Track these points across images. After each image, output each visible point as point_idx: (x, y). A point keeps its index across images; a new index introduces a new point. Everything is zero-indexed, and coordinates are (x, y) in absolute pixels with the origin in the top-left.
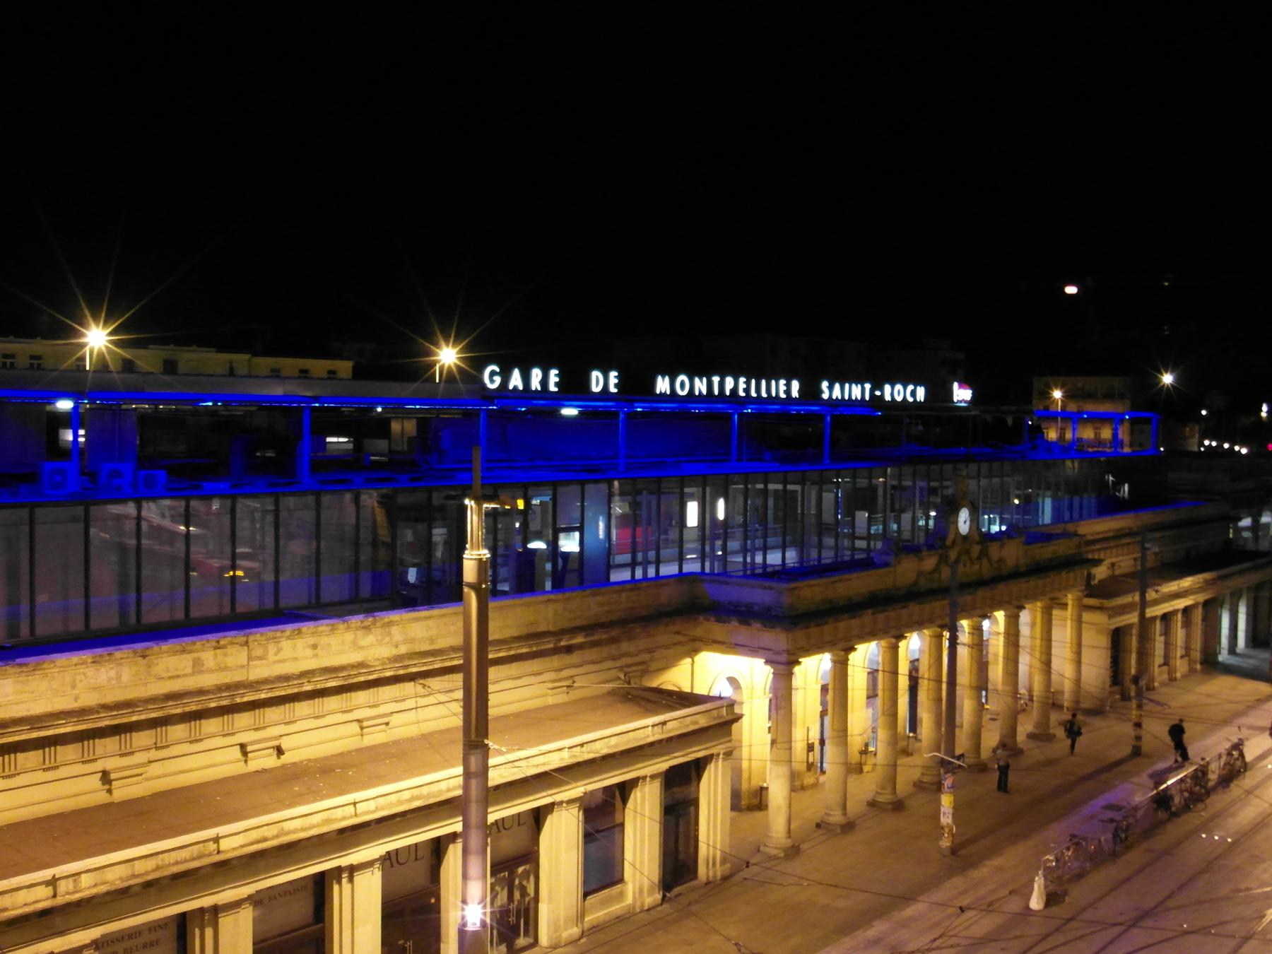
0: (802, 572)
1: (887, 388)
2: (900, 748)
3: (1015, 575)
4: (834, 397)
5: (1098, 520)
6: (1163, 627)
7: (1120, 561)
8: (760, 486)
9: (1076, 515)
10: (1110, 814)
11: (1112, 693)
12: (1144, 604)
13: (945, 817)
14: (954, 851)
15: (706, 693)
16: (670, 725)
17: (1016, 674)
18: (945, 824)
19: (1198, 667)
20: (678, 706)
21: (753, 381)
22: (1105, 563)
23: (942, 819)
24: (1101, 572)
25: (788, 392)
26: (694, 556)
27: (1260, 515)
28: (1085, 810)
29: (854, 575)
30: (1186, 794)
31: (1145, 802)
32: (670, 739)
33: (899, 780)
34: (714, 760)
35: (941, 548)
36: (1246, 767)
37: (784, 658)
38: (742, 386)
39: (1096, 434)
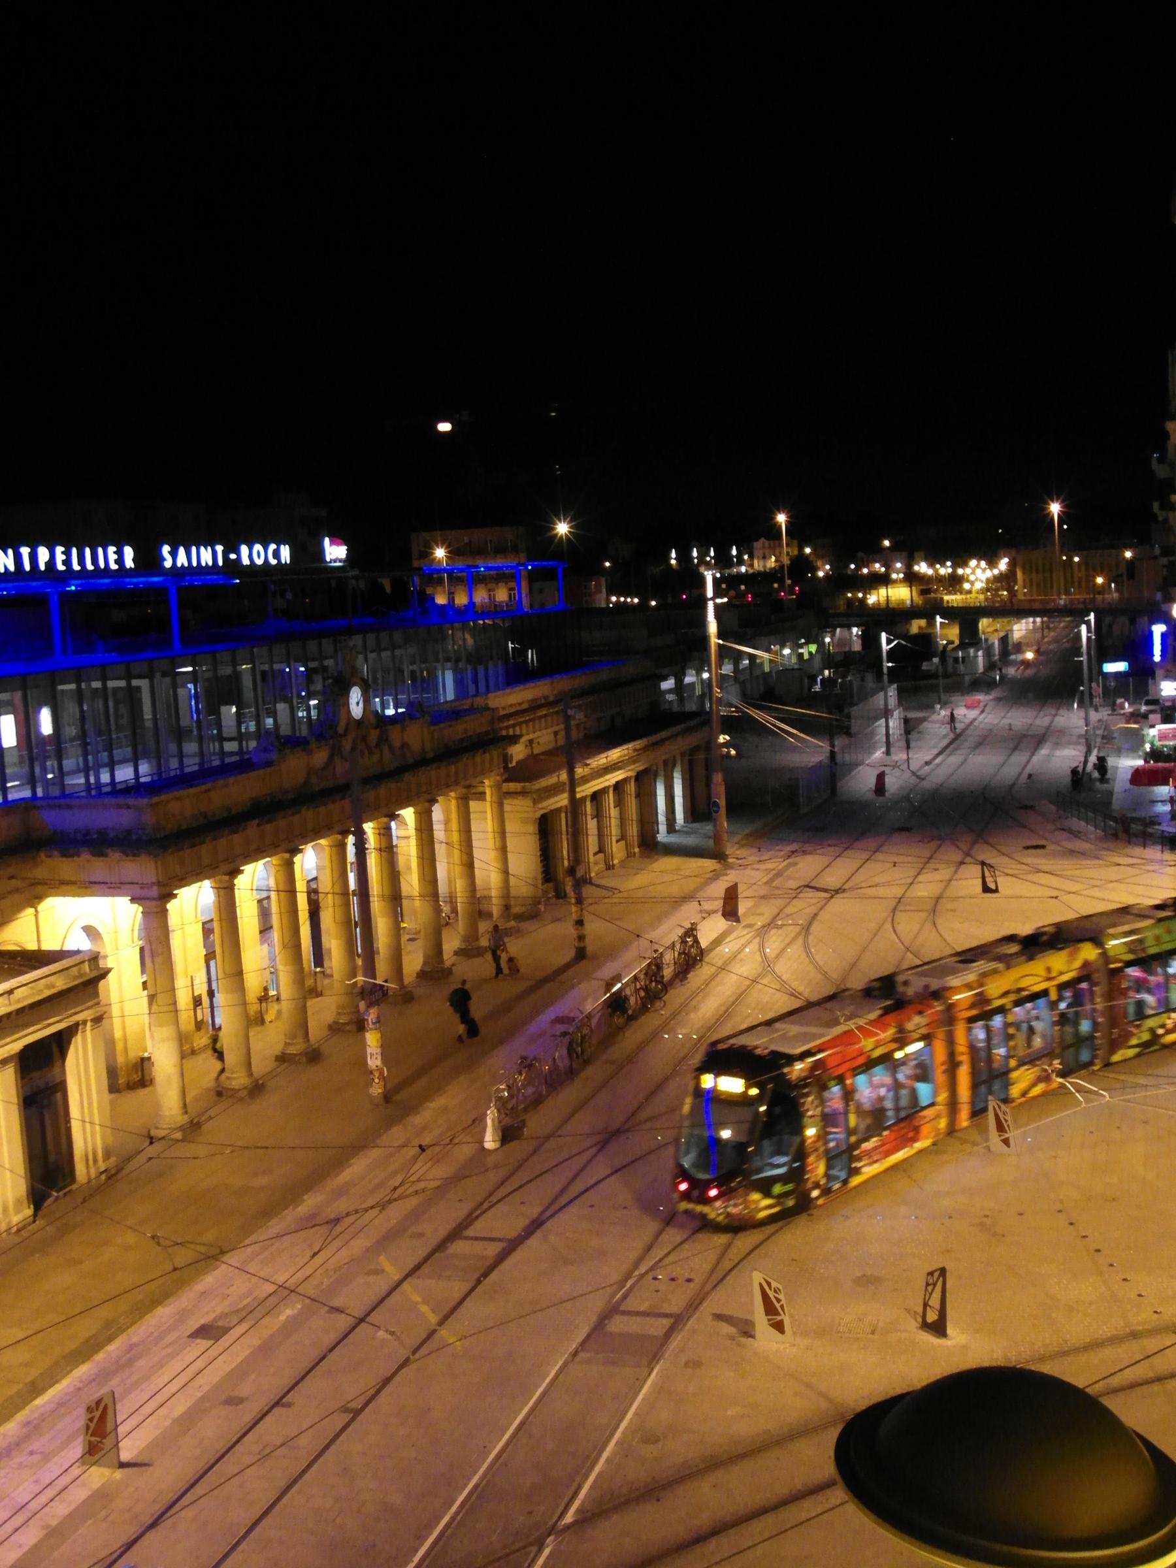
0: (160, 785)
1: (244, 549)
2: (308, 991)
3: (423, 762)
4: (179, 565)
5: (508, 691)
6: (595, 808)
8: (97, 684)
10: (560, 1028)
11: (545, 892)
12: (573, 783)
14: (387, 1097)
15: (58, 948)
16: (18, 994)
17: (434, 881)
18: (374, 1067)
19: (637, 850)
20: (25, 969)
21: (74, 551)
23: (369, 1062)
24: (518, 752)
25: (120, 561)
26: (17, 783)
28: (533, 1028)
29: (231, 780)
30: (642, 994)
31: (600, 1008)
32: (20, 1011)
34: (80, 1031)
35: (332, 737)
36: (702, 953)
37: (155, 891)
38: (60, 557)
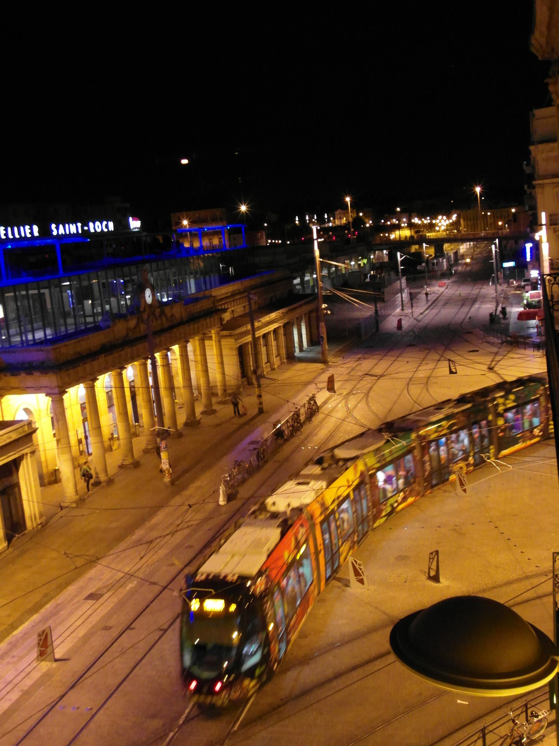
0: (57, 339)
1: (91, 224)
2: (132, 434)
3: (181, 323)
5: (221, 287)
7: (237, 309)
9: (208, 287)
12: (254, 330)
13: (165, 465)
14: (172, 483)
18: (165, 469)
19: (285, 361)
22: (228, 311)
24: (227, 316)
25: (32, 233)
27: (304, 276)
30: (291, 428)
33: (134, 450)
36: (318, 408)
39: (210, 243)
